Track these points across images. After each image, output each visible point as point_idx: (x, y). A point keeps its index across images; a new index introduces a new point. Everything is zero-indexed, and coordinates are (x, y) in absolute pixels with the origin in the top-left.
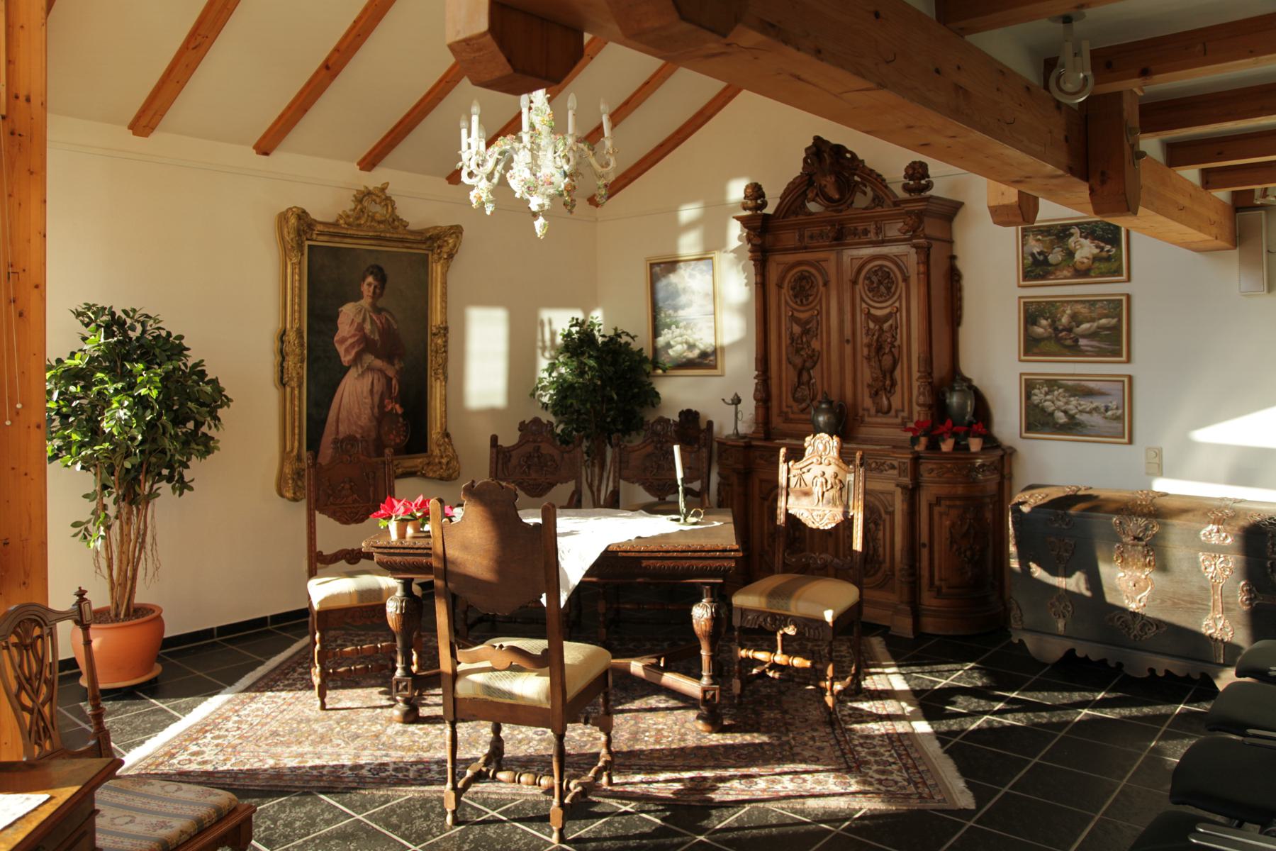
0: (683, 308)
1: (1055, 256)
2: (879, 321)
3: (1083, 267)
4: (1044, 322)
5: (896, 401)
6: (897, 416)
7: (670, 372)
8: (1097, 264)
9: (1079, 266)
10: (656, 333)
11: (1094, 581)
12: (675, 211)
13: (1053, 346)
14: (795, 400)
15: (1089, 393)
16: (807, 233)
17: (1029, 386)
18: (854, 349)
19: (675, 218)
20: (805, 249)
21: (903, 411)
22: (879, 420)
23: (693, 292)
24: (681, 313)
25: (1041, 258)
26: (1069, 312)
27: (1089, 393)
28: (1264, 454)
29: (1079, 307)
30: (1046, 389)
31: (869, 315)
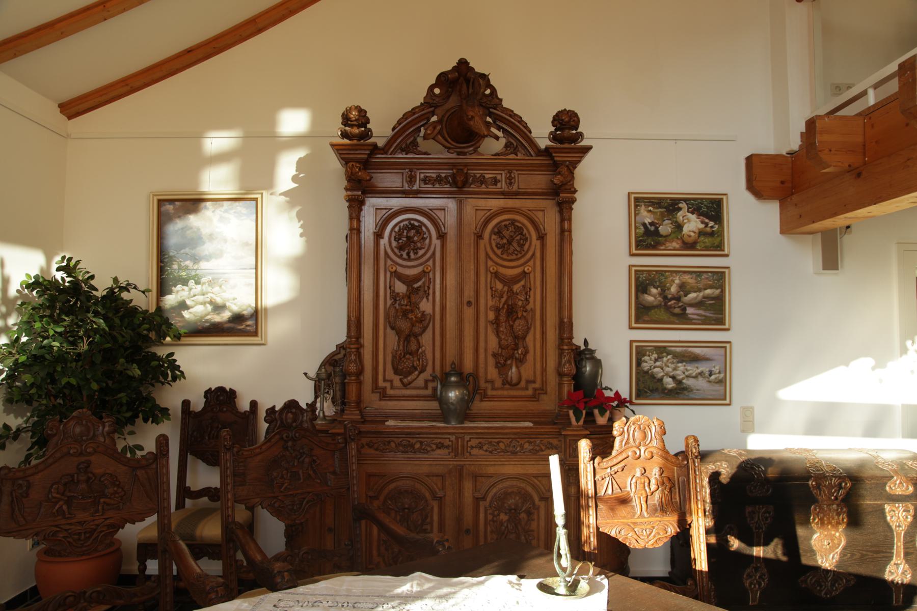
0: (207, 258)
1: (665, 228)
2: (509, 282)
3: (690, 240)
4: (654, 291)
5: (527, 371)
6: (426, 387)
7: (185, 340)
8: (702, 238)
9: (686, 239)
10: (163, 289)
11: (792, 546)
12: (198, 137)
13: (663, 314)
14: (396, 372)
15: (695, 359)
16: (420, 175)
17: (639, 352)
18: (477, 312)
19: (199, 148)
20: (416, 194)
21: (534, 382)
22: (505, 393)
23: (225, 241)
24: (203, 265)
25: (652, 228)
26: (677, 281)
27: (695, 359)
28: (832, 408)
29: (687, 278)
30: (655, 356)
31: (496, 275)
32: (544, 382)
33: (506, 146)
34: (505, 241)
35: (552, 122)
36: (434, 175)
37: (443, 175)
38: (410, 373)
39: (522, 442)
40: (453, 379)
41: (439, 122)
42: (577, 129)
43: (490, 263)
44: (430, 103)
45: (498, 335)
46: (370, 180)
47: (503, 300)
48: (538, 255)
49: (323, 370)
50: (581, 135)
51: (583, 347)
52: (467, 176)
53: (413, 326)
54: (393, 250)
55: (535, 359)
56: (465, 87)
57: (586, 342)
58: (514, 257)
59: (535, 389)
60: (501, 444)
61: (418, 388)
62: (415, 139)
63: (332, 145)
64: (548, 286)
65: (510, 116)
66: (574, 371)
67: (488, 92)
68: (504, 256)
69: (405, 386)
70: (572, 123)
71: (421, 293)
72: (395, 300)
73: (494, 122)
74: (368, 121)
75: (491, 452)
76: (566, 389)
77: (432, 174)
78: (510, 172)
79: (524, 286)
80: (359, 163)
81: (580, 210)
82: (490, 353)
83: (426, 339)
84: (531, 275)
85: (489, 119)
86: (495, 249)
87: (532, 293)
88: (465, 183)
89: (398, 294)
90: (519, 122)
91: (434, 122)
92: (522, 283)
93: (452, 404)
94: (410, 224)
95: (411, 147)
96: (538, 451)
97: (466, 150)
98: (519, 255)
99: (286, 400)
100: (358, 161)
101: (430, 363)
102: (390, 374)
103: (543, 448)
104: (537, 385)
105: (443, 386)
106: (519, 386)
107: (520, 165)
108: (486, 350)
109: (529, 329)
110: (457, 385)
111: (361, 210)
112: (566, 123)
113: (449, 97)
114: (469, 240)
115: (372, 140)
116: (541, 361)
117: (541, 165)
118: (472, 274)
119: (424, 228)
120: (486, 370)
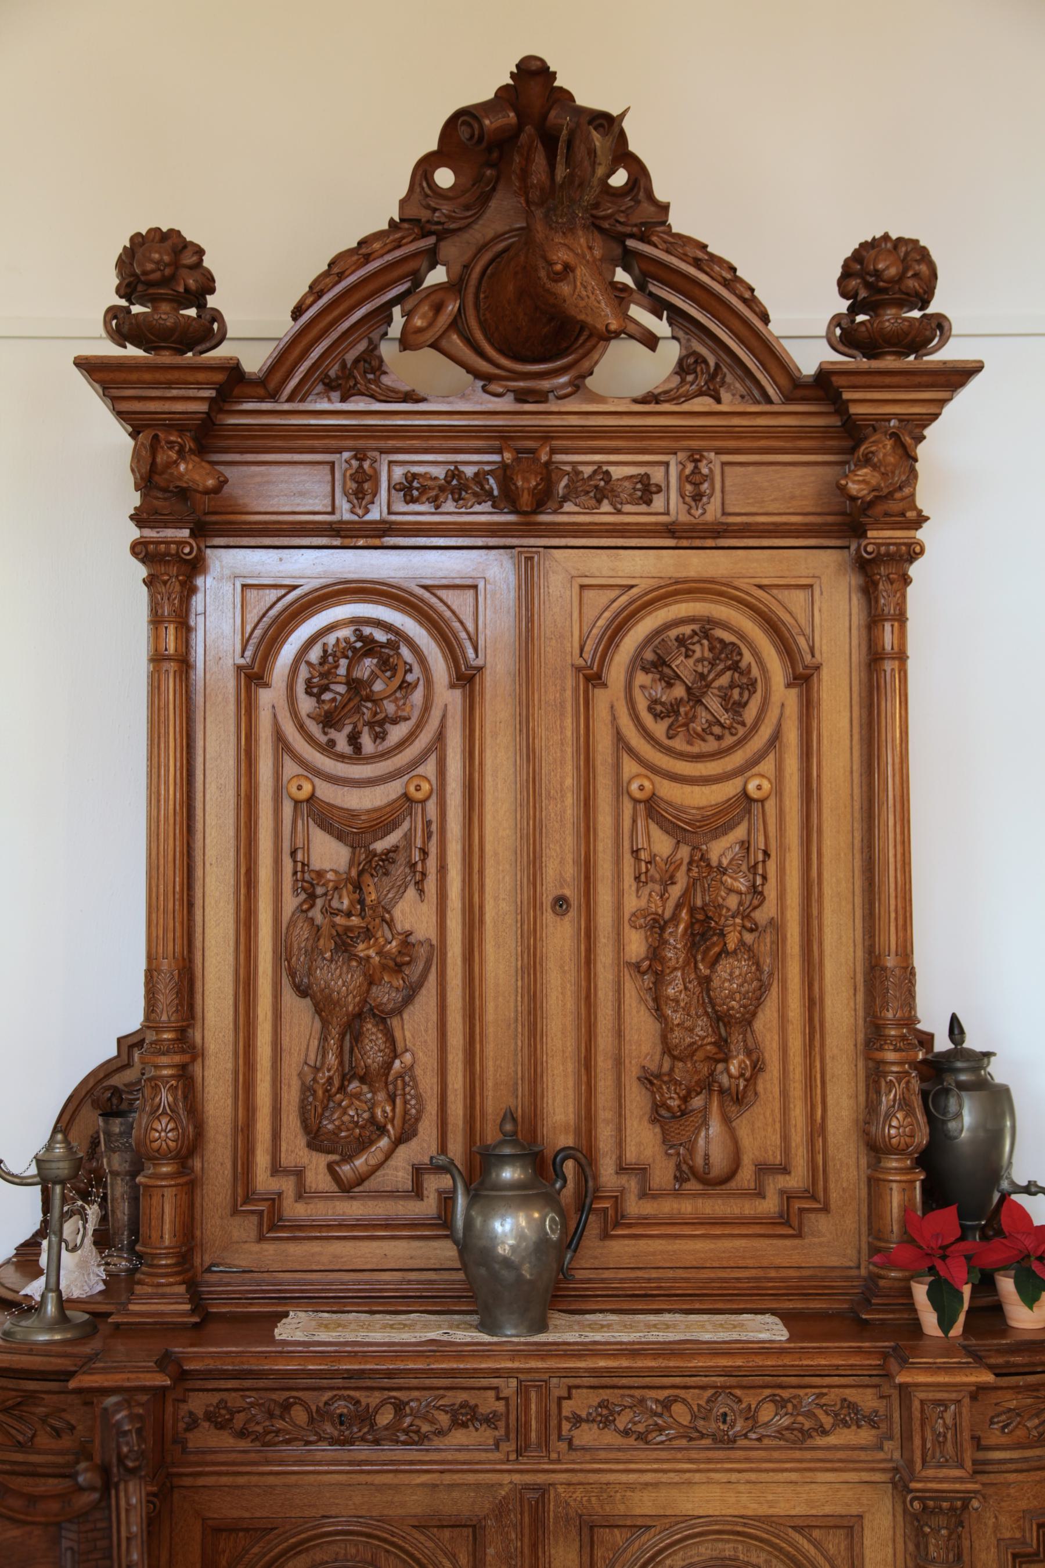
5: (759, 1133)
6: (417, 1192)
14: (316, 1140)
16: (390, 471)
22: (686, 1207)
32: (818, 1171)
33: (682, 368)
34: (679, 691)
35: (841, 282)
36: (439, 472)
37: (469, 471)
38: (363, 1145)
39: (750, 1399)
40: (508, 1174)
41: (455, 286)
42: (924, 304)
43: (630, 767)
44: (422, 222)
45: (658, 1011)
46: (217, 490)
47: (675, 892)
48: (792, 736)
49: (59, 1150)
50: (940, 325)
51: (942, 1044)
52: (548, 473)
53: (371, 981)
54: (301, 727)
55: (784, 1094)
56: (540, 160)
57: (956, 1028)
58: (712, 745)
59: (788, 1196)
60: (677, 1408)
61: (393, 1194)
62: (373, 348)
63: (88, 366)
64: (828, 843)
65: (697, 263)
66: (922, 1138)
67: (619, 179)
68: (679, 744)
69: (347, 1188)
70: (912, 284)
71: (399, 870)
72: (312, 897)
73: (642, 286)
74: (208, 285)
75: (641, 1437)
76: (895, 1200)
77: (433, 466)
78: (696, 457)
79: (746, 846)
80: (181, 429)
81: (931, 590)
82: (632, 1071)
83: (416, 1026)
84: (771, 806)
85: (622, 276)
86: (648, 719)
87: (772, 866)
88: (544, 498)
89: (320, 874)
90: (726, 284)
91: (438, 287)
92: (740, 832)
93: (506, 1262)
94: (360, 637)
95: (360, 375)
96: (806, 1434)
97: (546, 384)
98: (729, 740)
99: (842, 263)
100: (177, 424)
101: (432, 1108)
102: (294, 1148)
103: (827, 1421)
104: (796, 1180)
105: (474, 1196)
106: (733, 1184)
107: (730, 433)
108: (619, 1062)
109: (763, 989)
110: (522, 1196)
111: (193, 590)
112: (888, 284)
113: (484, 200)
114: (558, 689)
115: (223, 351)
116: (808, 1103)
117: (800, 433)
118: (569, 805)
119: (405, 652)
120: (620, 1130)
